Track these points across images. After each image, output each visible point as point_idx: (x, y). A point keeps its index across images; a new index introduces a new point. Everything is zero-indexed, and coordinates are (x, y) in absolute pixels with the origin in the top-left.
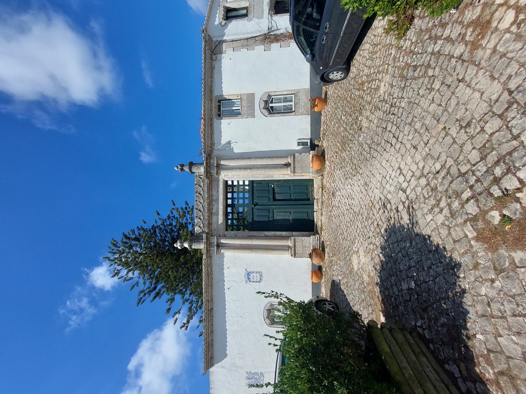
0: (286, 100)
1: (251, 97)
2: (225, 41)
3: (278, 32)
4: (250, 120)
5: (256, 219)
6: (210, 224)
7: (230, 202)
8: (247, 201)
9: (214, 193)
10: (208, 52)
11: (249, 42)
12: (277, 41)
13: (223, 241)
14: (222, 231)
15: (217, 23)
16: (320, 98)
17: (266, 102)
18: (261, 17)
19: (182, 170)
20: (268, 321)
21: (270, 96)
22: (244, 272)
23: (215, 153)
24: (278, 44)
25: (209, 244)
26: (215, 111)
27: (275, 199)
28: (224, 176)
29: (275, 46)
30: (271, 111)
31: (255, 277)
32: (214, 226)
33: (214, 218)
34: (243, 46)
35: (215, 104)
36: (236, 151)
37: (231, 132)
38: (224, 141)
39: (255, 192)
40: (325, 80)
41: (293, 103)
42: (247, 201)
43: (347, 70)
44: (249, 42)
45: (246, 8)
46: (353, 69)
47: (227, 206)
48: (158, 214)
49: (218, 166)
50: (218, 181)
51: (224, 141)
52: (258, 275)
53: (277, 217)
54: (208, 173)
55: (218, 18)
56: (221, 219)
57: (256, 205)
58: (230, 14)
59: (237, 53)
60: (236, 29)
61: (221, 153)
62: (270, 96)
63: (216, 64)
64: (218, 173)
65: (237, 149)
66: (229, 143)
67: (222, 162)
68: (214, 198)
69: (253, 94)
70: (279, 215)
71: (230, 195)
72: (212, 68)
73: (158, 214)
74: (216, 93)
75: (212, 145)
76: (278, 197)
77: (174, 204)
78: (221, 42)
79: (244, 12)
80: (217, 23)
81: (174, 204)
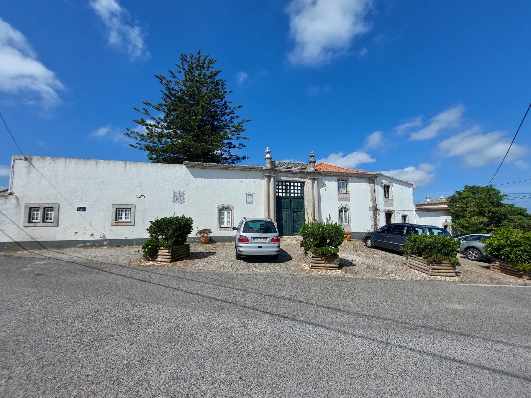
0: (346, 219)
1: (348, 199)
2: (375, 186)
3: (378, 215)
4: (337, 198)
5: (282, 200)
6: (281, 171)
7: (292, 184)
8: (292, 195)
9: (298, 175)
10: (370, 176)
11: (374, 199)
12: (374, 214)
13: (272, 180)
14: (277, 179)
15: (383, 181)
16: (350, 238)
17: (345, 208)
18: (385, 206)
19: (312, 156)
20: (221, 207)
21: (348, 210)
22: (252, 192)
23: (320, 177)
24: (372, 215)
25: (270, 171)
26: (341, 178)
27: (294, 212)
28: (308, 183)
29: (371, 213)
30: (341, 211)
31: (250, 199)
32: (279, 174)
33: (284, 174)
34: (372, 195)
35: (345, 178)
36: (321, 189)
37: (331, 186)
38: (326, 182)
39: (298, 200)
40: (365, 240)
41: (123, 220)
42: (292, 195)
43: (372, 247)
44: (374, 199)
45: (388, 197)
46: (373, 249)
47: (290, 182)
48: (240, 107)
49: (314, 179)
50: (305, 178)
51: (326, 182)
52: (251, 201)
53: (283, 213)
54: (311, 173)
55: (385, 182)
56: (283, 178)
57: (291, 201)
58: (386, 188)
59: (369, 192)
60: (380, 190)
61: (320, 180)
62: (348, 210)
63: (364, 180)
64: (310, 179)
65: (321, 190)
66: (325, 186)
67: (316, 181)
68: (296, 175)
69: (349, 201)
70: (285, 215)
71: (296, 184)
72: (362, 178)
73: (240, 107)
74: (350, 179)
75: (325, 176)
76: (295, 214)
77: (247, 121)
78: (374, 183)
79: (387, 196)
80: (383, 181)
81: (247, 121)
